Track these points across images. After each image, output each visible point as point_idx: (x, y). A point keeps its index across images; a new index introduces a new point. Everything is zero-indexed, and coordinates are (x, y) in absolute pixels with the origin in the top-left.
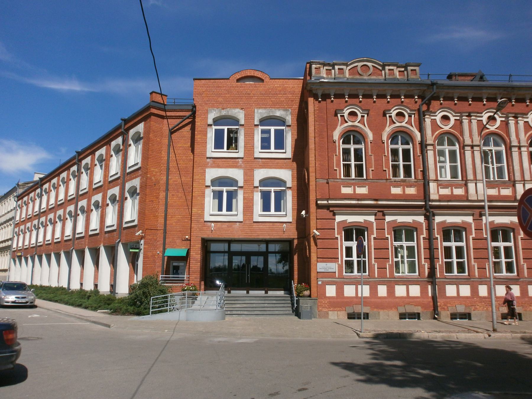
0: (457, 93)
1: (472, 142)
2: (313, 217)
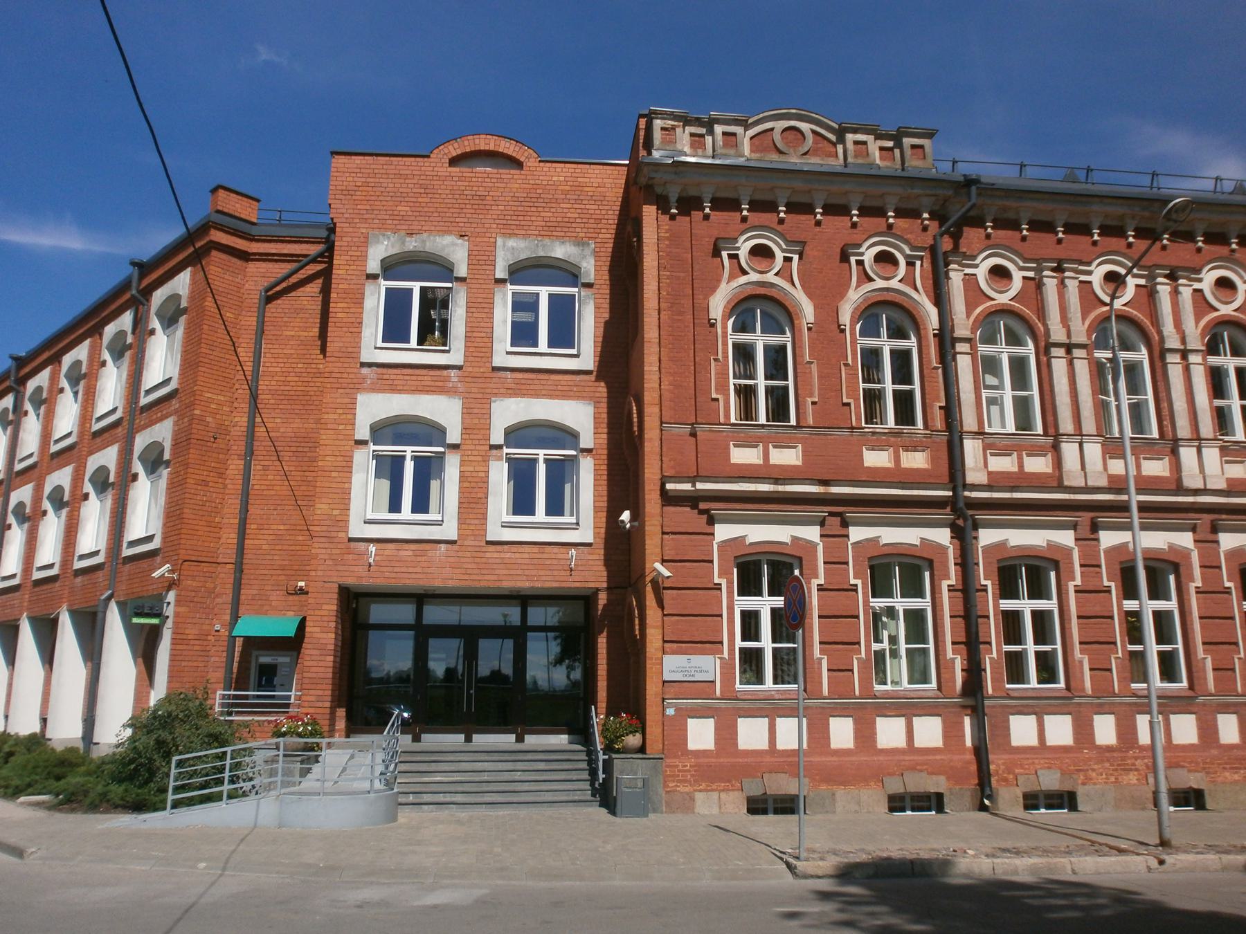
0: (1028, 209)
1: (1069, 336)
2: (652, 527)
